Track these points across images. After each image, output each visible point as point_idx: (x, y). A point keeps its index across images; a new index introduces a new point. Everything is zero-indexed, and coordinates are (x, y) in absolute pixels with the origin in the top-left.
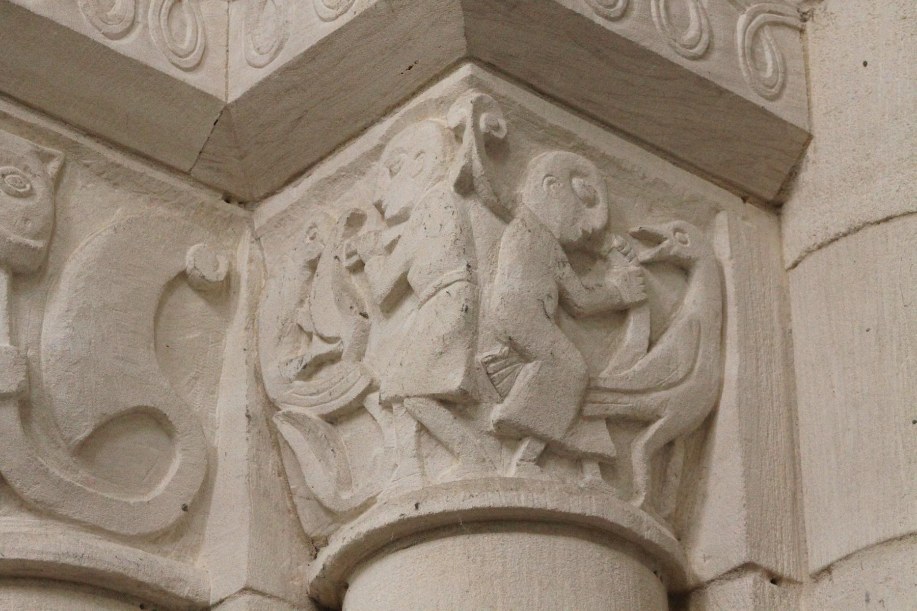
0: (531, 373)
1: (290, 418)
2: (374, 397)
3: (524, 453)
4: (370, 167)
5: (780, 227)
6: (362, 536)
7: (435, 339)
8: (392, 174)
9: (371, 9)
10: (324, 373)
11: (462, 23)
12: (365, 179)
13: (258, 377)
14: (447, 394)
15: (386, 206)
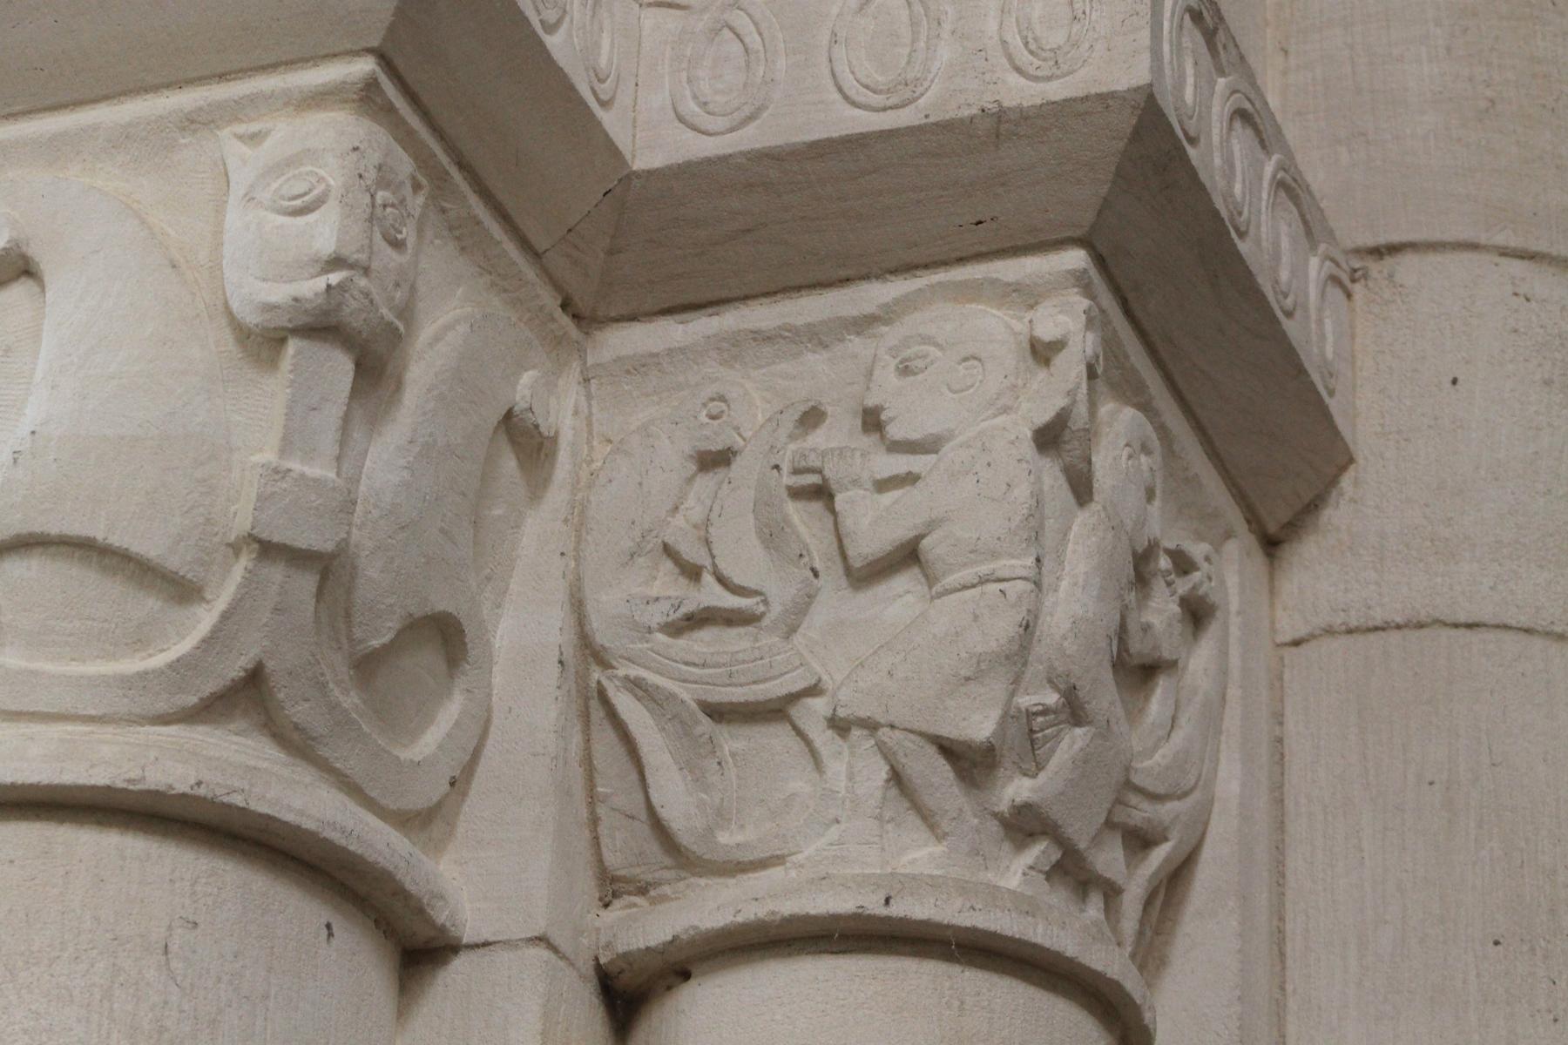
0: (1079, 744)
1: (636, 686)
2: (819, 705)
3: (1038, 858)
4: (842, 340)
5: (1272, 578)
6: (778, 917)
7: (963, 655)
8: (905, 370)
9: (962, 120)
10: (706, 634)
11: (1105, 189)
12: (826, 355)
13: (578, 606)
14: (963, 743)
15: (891, 419)
